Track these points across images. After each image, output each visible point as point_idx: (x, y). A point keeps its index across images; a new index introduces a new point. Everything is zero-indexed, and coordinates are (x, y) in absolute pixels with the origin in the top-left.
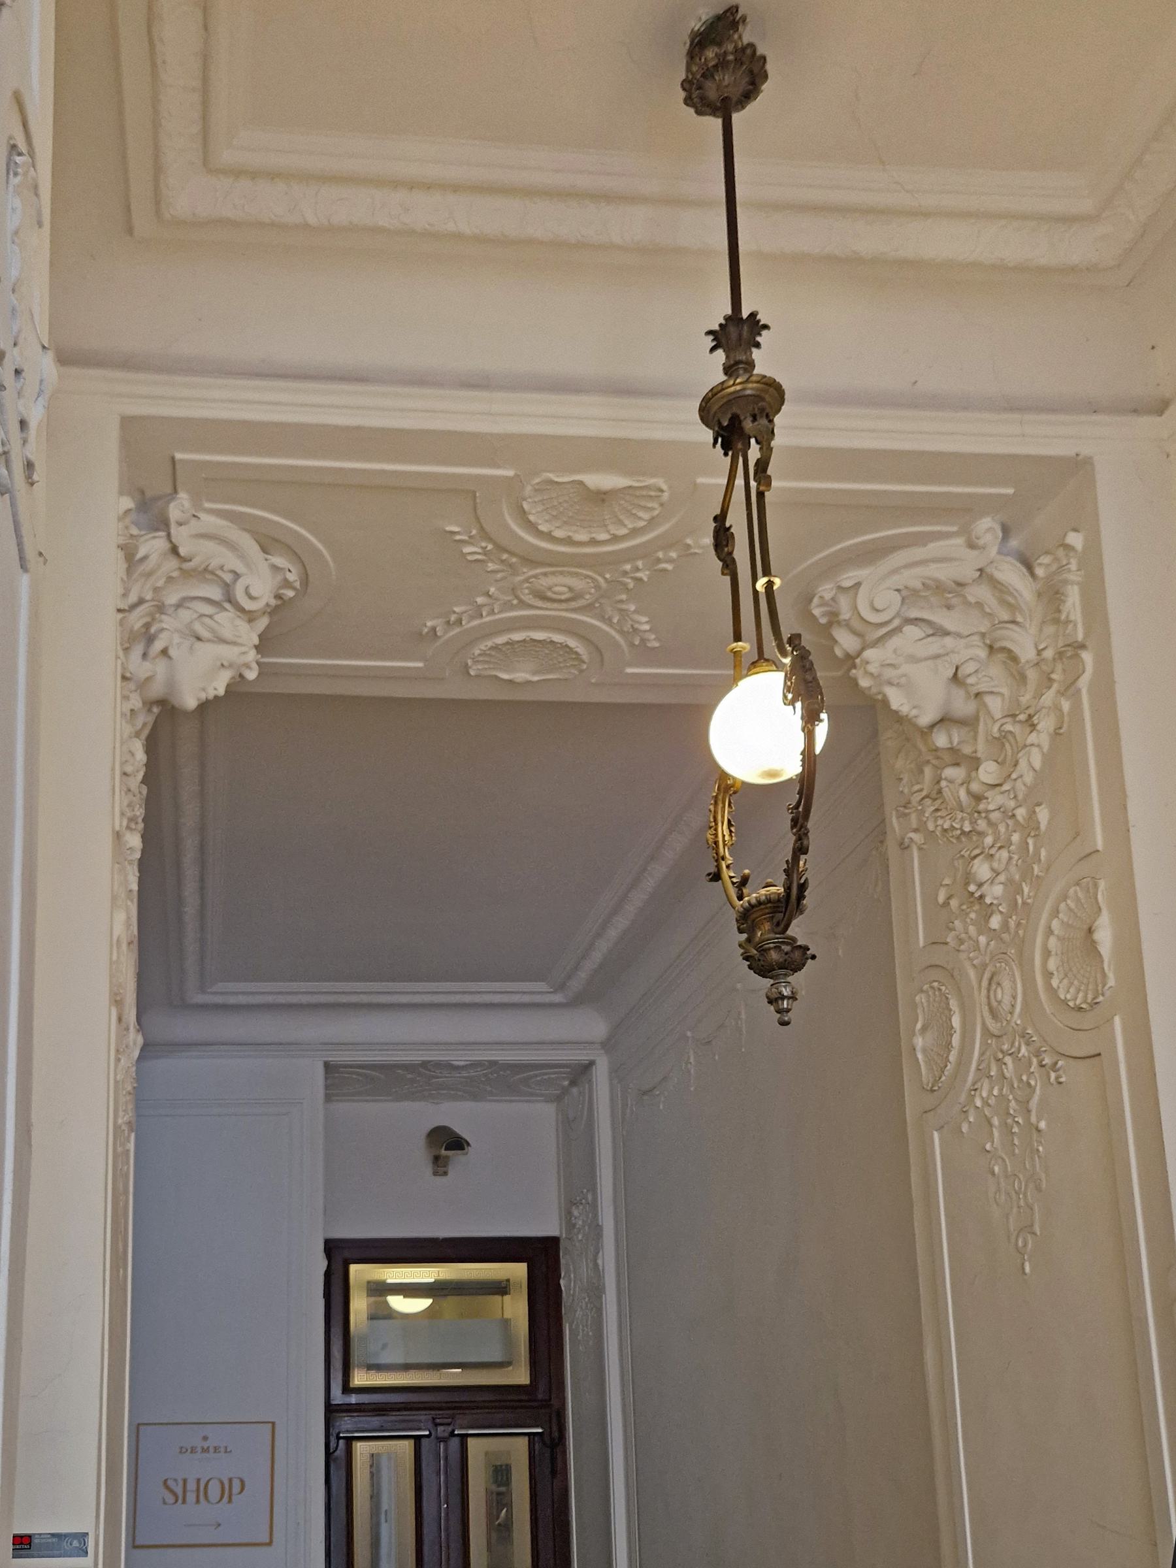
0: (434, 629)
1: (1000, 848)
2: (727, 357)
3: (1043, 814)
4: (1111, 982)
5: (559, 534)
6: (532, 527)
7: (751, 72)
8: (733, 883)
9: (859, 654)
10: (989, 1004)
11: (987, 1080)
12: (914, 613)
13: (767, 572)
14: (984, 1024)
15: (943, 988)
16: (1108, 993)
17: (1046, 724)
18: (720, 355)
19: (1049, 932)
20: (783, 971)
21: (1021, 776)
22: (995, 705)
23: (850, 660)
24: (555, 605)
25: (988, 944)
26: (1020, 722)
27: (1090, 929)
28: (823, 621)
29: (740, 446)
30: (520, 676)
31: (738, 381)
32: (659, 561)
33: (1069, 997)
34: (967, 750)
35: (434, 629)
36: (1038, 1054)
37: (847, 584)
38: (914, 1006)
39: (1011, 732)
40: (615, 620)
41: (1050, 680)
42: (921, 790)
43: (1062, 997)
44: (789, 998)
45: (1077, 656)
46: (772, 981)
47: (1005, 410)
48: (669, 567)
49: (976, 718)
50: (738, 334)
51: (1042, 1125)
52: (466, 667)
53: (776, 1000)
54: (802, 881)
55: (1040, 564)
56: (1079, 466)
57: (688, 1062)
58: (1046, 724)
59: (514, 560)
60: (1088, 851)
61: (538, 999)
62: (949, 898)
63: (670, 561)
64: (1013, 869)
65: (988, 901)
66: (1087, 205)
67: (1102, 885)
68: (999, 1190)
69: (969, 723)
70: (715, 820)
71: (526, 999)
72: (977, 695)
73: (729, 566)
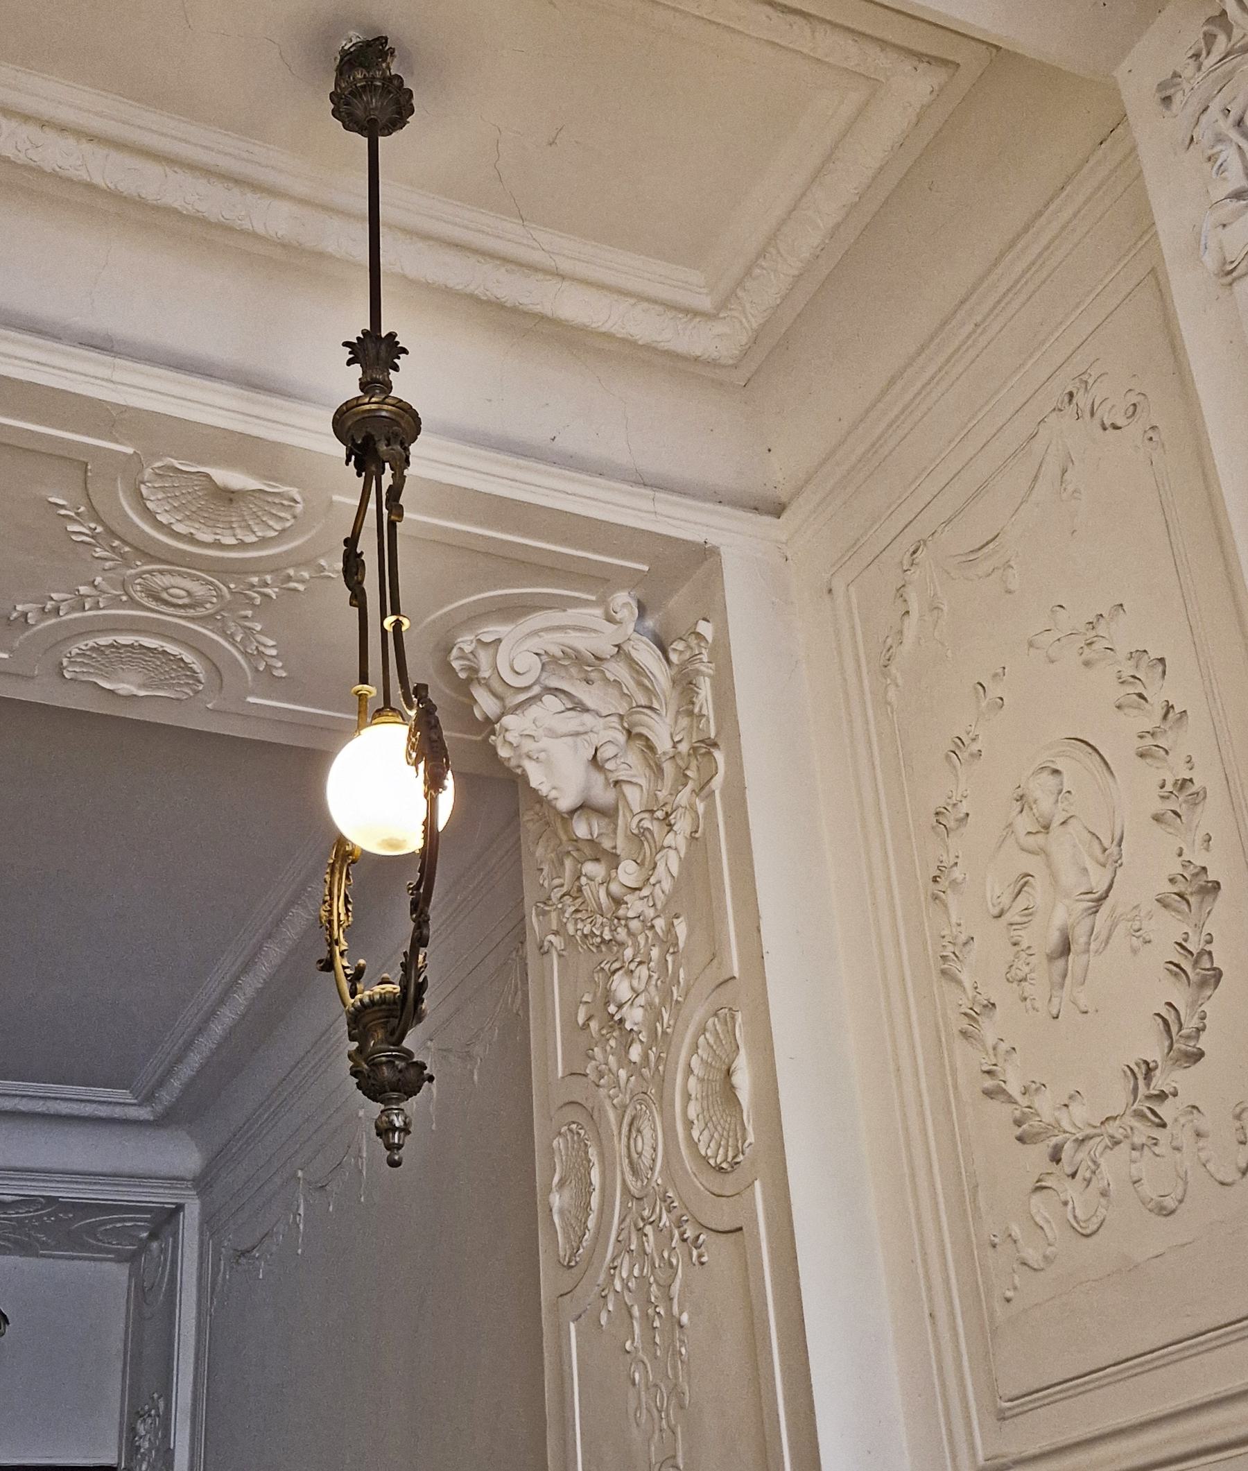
0: (25, 615)
1: (640, 963)
2: (364, 372)
3: (681, 928)
4: (751, 1138)
5: (179, 528)
6: (150, 516)
7: (397, 102)
8: (347, 976)
9: (499, 719)
10: (629, 1156)
11: (627, 1256)
12: (554, 683)
13: (396, 611)
14: (624, 1181)
15: (582, 1132)
16: (747, 1151)
17: (683, 825)
18: (357, 370)
19: (689, 1071)
20: (395, 1095)
21: (659, 882)
22: (631, 793)
23: (489, 725)
24: (171, 610)
25: (628, 1080)
26: (658, 819)
27: (728, 1070)
28: (463, 675)
29: (373, 468)
30: (124, 688)
31: (373, 400)
32: (289, 579)
33: (709, 1154)
34: (607, 844)
35: (25, 615)
36: (679, 1224)
37: (487, 638)
38: (551, 1151)
39: (648, 829)
40: (238, 639)
41: (686, 776)
42: (562, 885)
43: (703, 1153)
44: (400, 1130)
45: (710, 753)
46: (382, 1107)
47: (636, 483)
48: (301, 587)
49: (617, 809)
50: (375, 352)
51: (685, 1318)
52: (61, 668)
53: (387, 1131)
54: (421, 980)
55: (674, 650)
56: (704, 555)
57: (297, 1214)
58: (683, 825)
59: (127, 549)
60: (727, 977)
61: (118, 1112)
62: (589, 1019)
63: (302, 581)
64: (652, 989)
65: (628, 1026)
66: (705, 302)
67: (739, 1017)
68: (639, 1407)
69: (608, 813)
70: (331, 894)
71: (103, 1111)
72: (616, 783)
73: (358, 598)
